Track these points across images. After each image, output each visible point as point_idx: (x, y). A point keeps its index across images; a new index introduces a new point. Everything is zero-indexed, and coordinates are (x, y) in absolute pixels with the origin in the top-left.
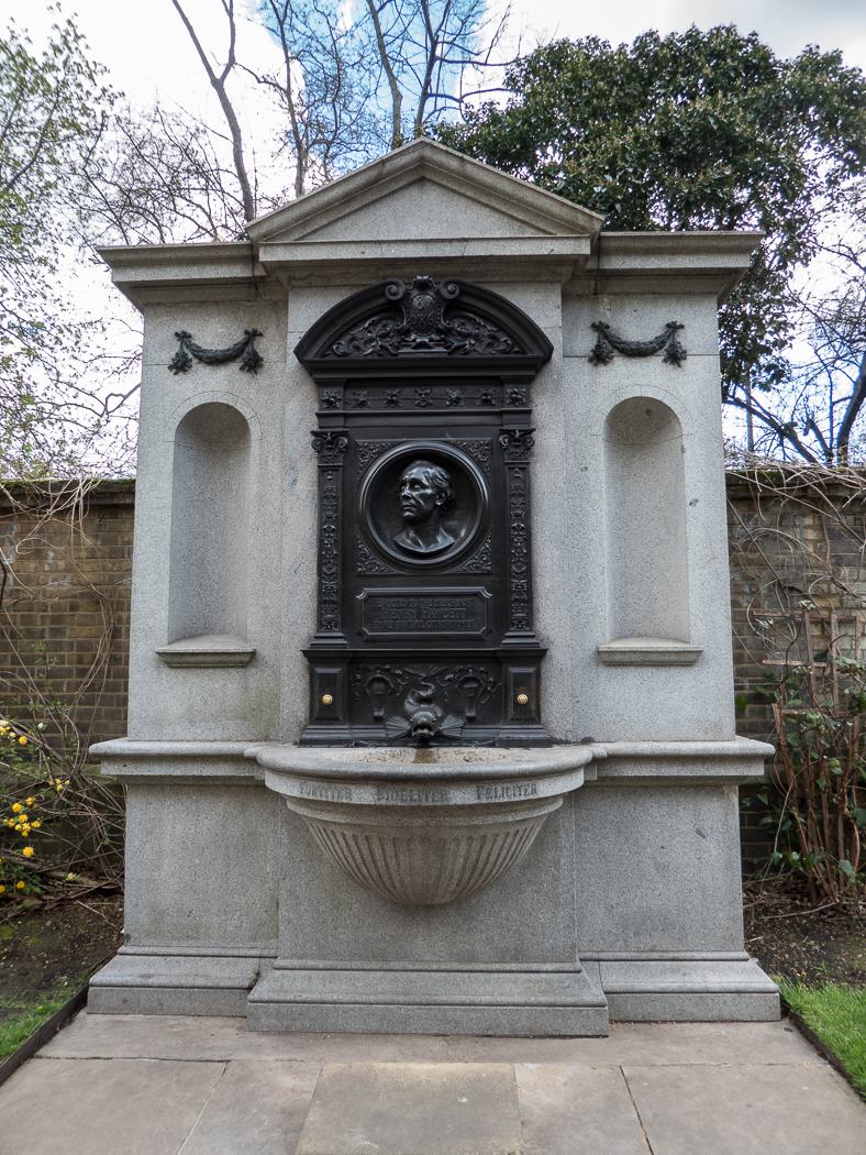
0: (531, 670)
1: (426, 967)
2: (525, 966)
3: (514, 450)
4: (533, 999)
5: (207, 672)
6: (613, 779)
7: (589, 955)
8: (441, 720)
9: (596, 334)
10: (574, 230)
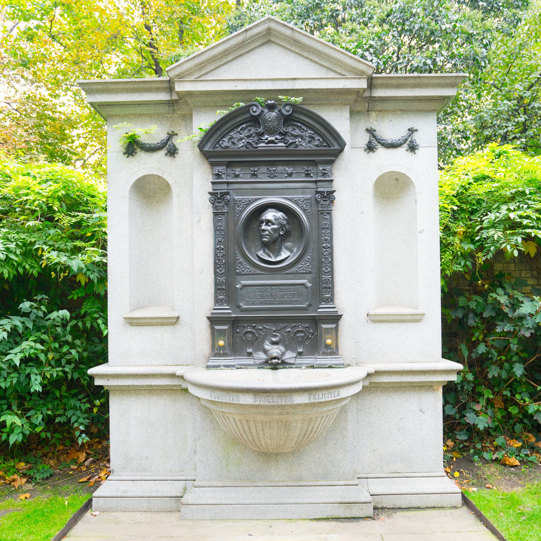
0: (334, 326)
1: (276, 484)
2: (329, 483)
3: (324, 203)
4: (333, 500)
5: (152, 328)
6: (376, 383)
7: (362, 475)
8: (283, 354)
9: (369, 135)
10: (359, 74)
